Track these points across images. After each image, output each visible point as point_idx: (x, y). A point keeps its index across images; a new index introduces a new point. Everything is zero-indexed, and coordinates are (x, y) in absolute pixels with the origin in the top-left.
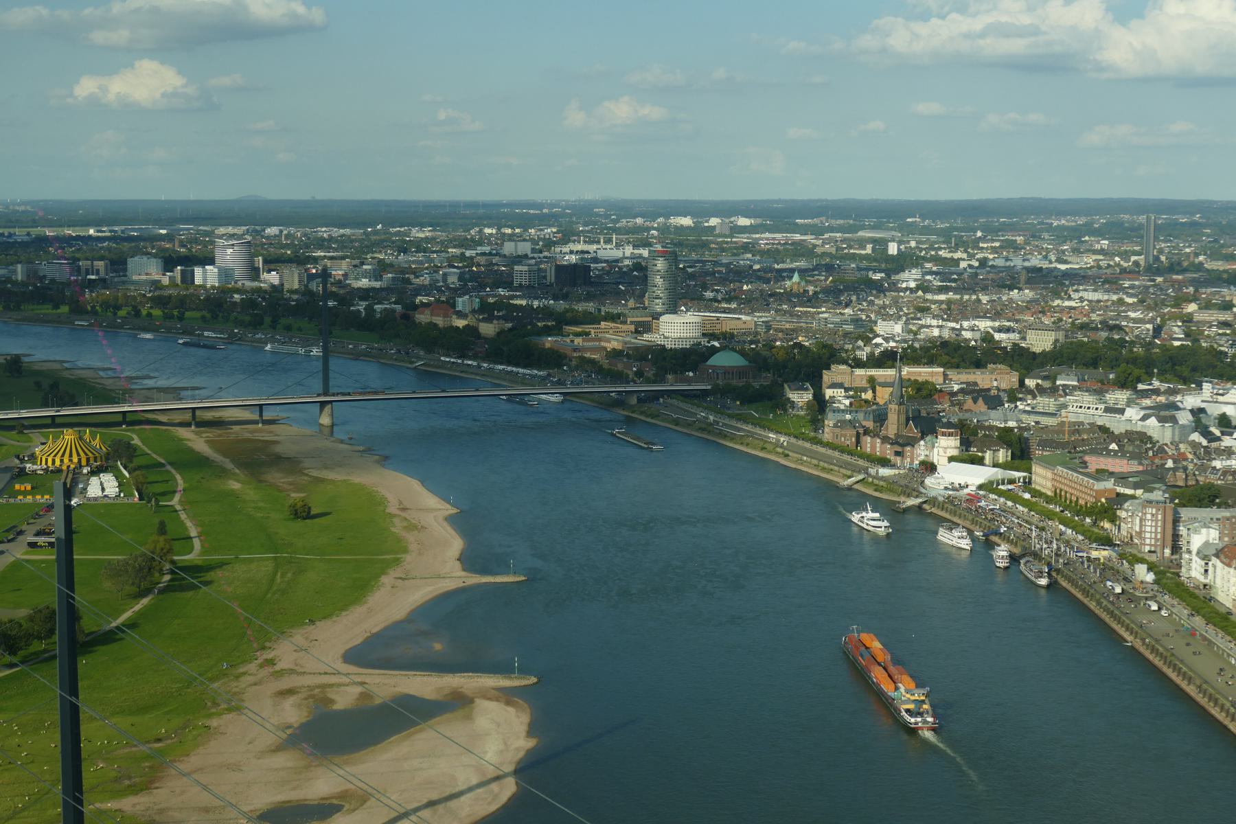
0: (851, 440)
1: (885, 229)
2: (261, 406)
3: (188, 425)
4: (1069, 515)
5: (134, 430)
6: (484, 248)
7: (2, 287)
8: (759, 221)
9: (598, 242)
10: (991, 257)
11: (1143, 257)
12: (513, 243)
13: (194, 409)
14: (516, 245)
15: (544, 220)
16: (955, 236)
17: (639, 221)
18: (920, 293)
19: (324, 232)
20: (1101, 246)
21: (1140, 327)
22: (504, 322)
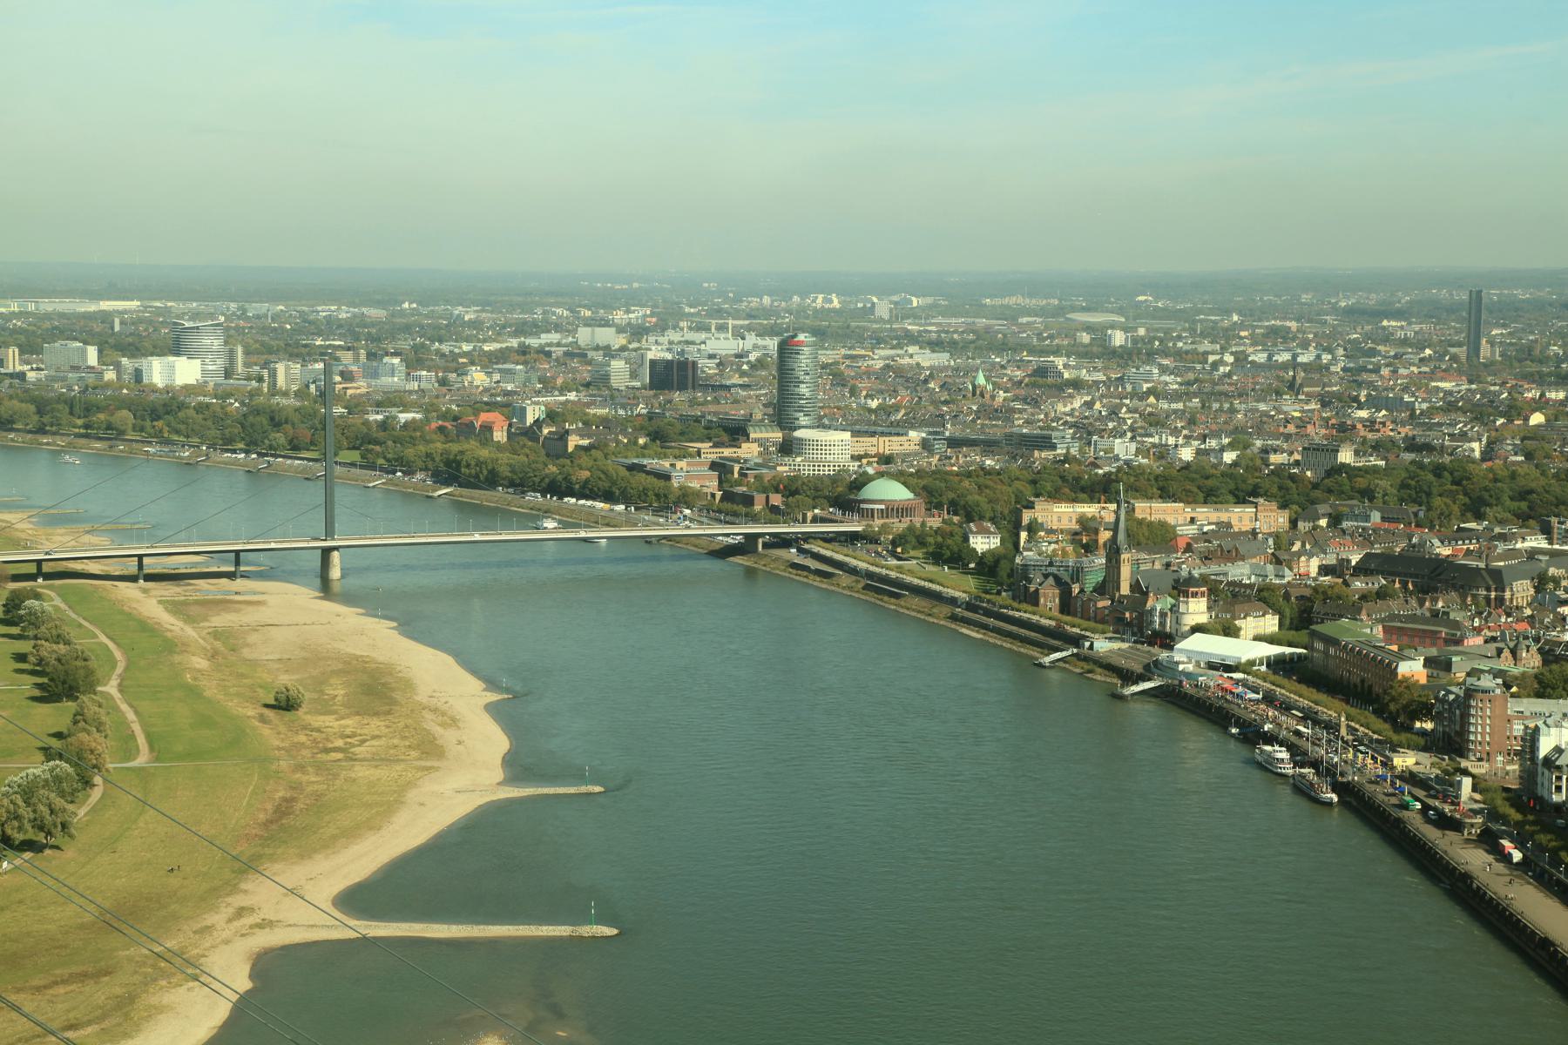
0: (1054, 601)
1: (1102, 312)
2: (237, 553)
3: (133, 579)
4: (19, 323)
5: (52, 585)
6: (550, 336)
7: (3, 310)
8: (929, 300)
9: (708, 329)
10: (1251, 350)
11: (1465, 348)
12: (589, 329)
13: (140, 557)
14: (593, 332)
15: (630, 300)
16: (1201, 321)
17: (766, 300)
18: (1152, 400)
19: (323, 311)
20: (1406, 334)
21: (1461, 446)
22: (578, 438)
